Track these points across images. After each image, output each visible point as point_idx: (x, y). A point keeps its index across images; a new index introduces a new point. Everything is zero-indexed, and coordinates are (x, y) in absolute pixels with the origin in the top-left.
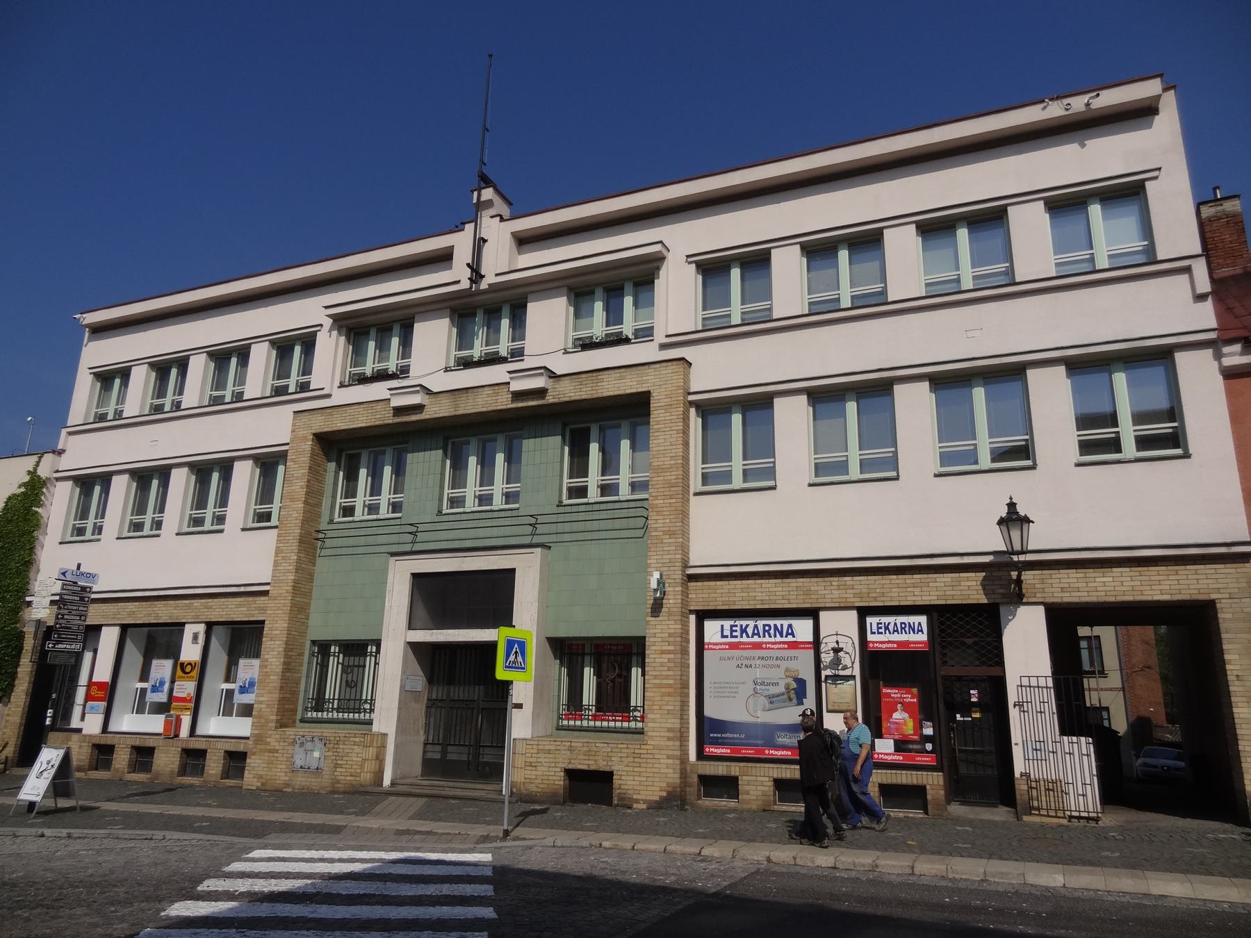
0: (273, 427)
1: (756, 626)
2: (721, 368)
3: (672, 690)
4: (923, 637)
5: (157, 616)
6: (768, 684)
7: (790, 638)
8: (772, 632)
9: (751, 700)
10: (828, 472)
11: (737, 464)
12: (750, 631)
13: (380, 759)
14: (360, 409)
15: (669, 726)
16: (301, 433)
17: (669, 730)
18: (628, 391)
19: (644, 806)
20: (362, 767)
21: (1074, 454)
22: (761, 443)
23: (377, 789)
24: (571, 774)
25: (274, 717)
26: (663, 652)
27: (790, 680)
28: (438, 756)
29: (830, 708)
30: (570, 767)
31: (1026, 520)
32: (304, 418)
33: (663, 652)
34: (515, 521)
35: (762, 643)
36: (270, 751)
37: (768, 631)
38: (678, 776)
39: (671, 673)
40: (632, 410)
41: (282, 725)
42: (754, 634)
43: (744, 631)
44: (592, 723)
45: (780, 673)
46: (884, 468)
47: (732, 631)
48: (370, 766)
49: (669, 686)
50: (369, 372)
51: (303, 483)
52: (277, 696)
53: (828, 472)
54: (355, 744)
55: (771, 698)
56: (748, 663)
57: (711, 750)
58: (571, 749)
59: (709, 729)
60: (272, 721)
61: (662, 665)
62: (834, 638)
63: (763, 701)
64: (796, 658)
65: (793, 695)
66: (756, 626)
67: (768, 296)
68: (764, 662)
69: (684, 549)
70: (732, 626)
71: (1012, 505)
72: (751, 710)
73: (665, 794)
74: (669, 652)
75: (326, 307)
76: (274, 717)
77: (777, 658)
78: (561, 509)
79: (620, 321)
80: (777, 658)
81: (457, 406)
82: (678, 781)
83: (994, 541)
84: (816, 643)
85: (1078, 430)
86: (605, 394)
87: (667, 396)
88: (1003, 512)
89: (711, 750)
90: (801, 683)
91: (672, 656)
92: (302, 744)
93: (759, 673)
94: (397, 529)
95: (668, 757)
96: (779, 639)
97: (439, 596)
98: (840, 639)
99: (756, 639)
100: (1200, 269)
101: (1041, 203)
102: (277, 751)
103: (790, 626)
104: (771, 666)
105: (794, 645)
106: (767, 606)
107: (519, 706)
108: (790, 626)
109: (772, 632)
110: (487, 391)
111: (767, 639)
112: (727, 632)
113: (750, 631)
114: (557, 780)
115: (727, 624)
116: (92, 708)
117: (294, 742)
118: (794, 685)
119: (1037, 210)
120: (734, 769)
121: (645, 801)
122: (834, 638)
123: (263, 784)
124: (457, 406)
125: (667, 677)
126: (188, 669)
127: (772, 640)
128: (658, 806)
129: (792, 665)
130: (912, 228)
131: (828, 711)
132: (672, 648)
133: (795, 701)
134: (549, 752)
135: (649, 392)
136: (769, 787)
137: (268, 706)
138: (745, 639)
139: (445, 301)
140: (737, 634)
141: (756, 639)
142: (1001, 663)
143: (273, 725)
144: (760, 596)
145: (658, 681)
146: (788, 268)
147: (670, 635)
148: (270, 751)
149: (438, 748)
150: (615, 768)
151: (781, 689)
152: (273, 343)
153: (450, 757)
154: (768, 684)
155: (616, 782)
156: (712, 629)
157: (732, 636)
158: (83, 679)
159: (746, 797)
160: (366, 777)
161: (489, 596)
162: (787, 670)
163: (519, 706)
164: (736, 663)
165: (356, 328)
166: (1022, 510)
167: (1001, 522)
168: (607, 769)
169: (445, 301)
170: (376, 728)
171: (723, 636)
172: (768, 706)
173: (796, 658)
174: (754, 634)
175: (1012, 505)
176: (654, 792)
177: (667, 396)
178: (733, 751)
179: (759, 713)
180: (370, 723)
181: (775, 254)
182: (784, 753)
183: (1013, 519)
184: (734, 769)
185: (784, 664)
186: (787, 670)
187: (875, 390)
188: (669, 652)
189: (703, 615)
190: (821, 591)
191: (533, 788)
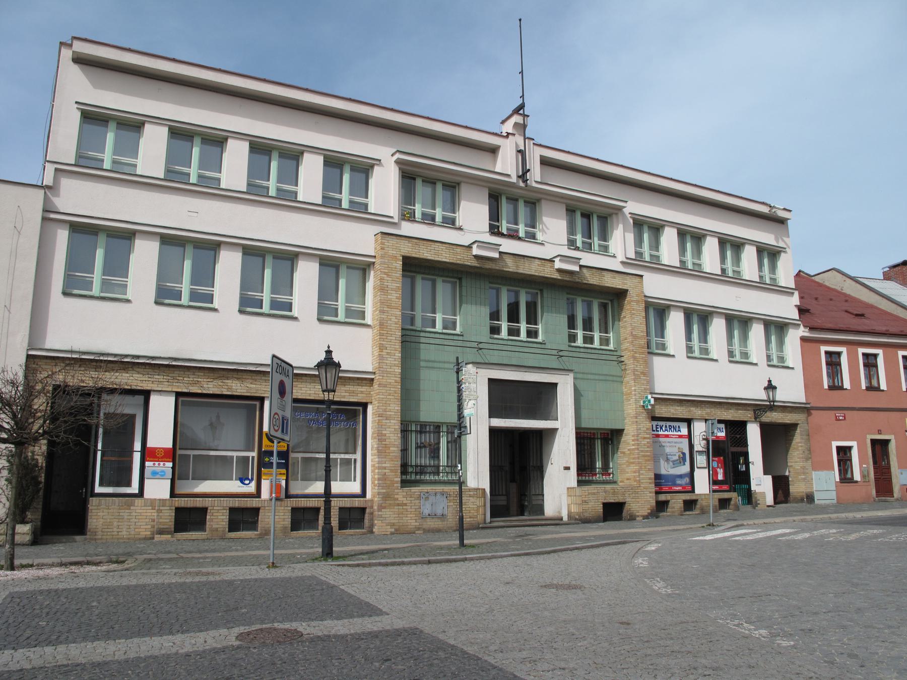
2: (657, 286)
4: (723, 434)
5: (229, 389)
7: (679, 433)
10: (165, 295)
11: (97, 276)
22: (118, 266)
26: (645, 438)
31: (775, 388)
32: (392, 241)
33: (645, 438)
36: (398, 505)
40: (613, 299)
41: (405, 483)
45: (676, 450)
46: (202, 300)
49: (648, 456)
53: (165, 295)
60: (397, 482)
67: (135, 154)
69: (650, 381)
71: (770, 381)
81: (517, 266)
83: (762, 395)
84: (689, 436)
88: (766, 384)
90: (684, 454)
92: (427, 498)
94: (460, 343)
97: (503, 397)
100: (796, 294)
102: (406, 505)
105: (681, 436)
110: (537, 262)
114: (600, 509)
116: (155, 473)
117: (419, 498)
119: (245, 146)
123: (396, 530)
125: (647, 451)
128: (645, 517)
129: (680, 446)
134: (594, 494)
135: (627, 290)
137: (392, 471)
139: (562, 198)
142: (746, 445)
143: (399, 485)
146: (236, 156)
148: (398, 505)
149: (504, 498)
150: (628, 500)
158: (137, 446)
161: (539, 398)
166: (773, 384)
167: (765, 388)
169: (562, 198)
175: (770, 381)
176: (646, 512)
181: (147, 127)
183: (770, 387)
187: (209, 248)
190: (697, 412)
191: (587, 515)
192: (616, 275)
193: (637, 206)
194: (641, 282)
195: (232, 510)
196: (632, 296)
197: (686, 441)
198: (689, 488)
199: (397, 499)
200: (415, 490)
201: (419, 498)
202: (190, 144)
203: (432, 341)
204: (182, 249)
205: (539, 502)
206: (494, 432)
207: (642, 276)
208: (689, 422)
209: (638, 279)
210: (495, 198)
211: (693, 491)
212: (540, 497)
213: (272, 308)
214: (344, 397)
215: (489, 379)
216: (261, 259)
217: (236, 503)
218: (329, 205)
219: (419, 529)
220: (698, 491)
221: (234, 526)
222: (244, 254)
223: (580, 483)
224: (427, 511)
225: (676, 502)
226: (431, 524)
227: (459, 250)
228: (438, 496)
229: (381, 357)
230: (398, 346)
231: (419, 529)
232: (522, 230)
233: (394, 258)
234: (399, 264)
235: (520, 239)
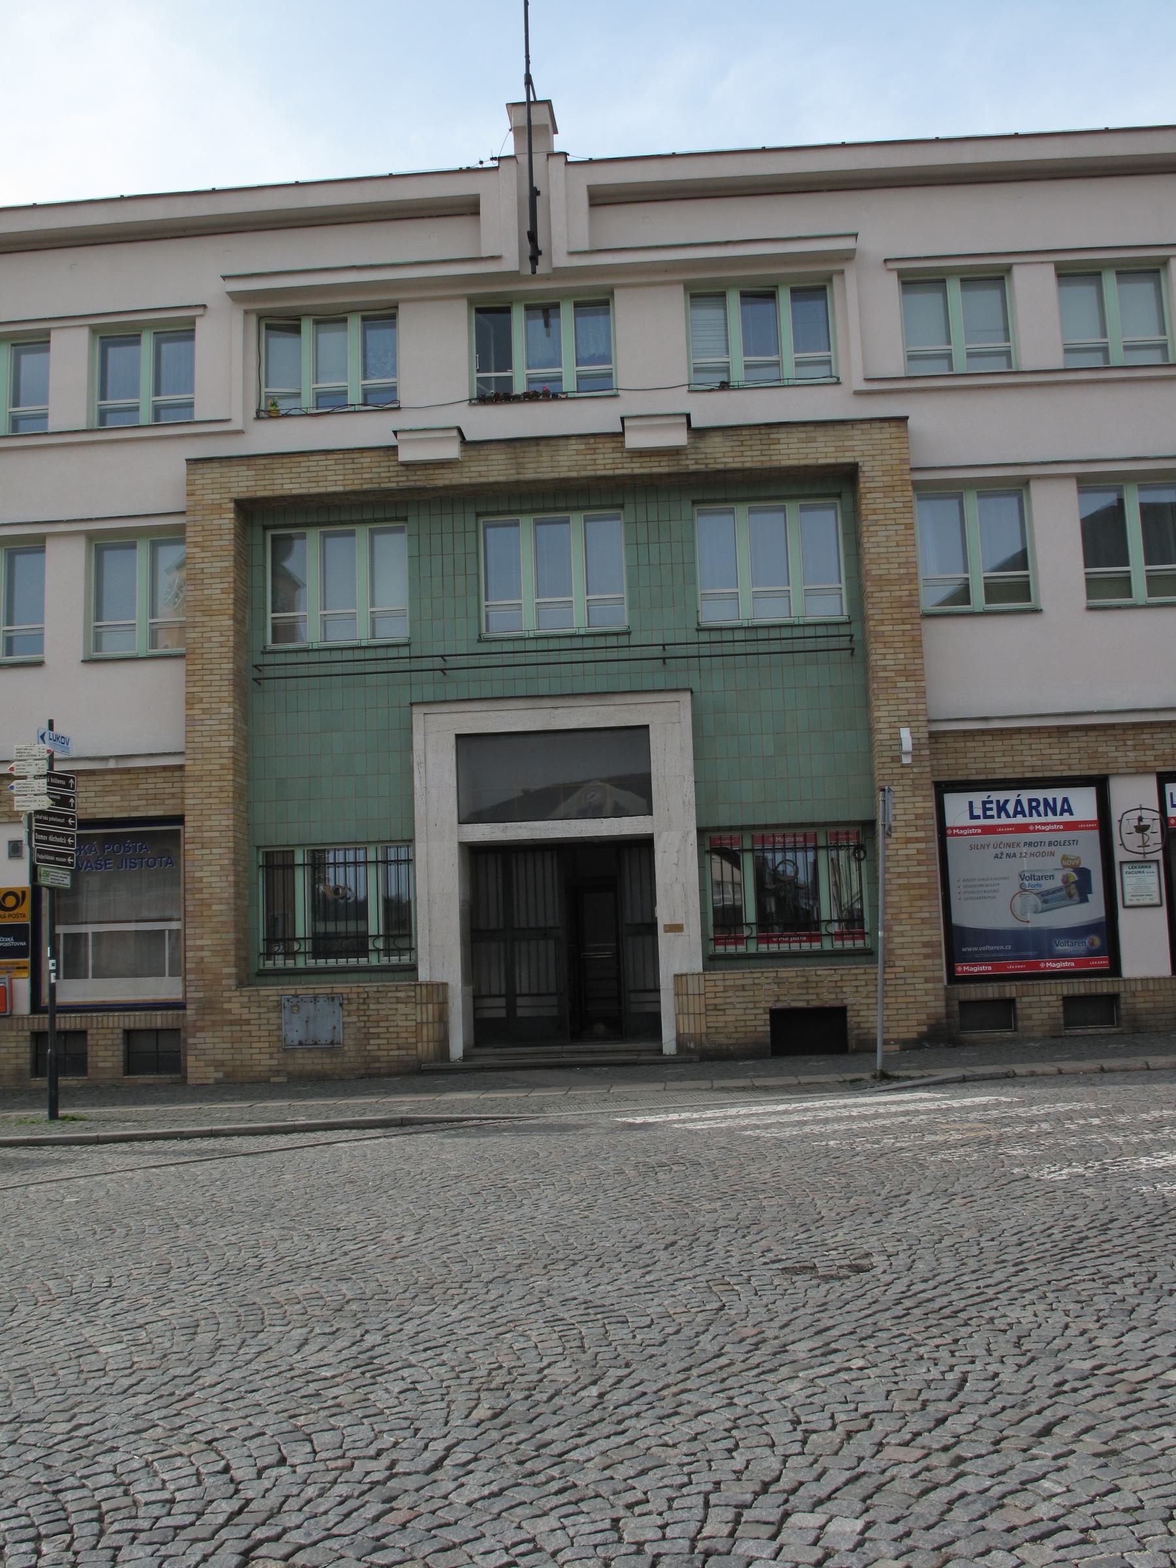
0: (144, 479)
1: (1019, 802)
3: (925, 892)
6: (1040, 878)
7: (1066, 817)
8: (1041, 808)
9: (1018, 900)
12: (1010, 808)
13: (442, 1019)
14: (330, 461)
15: (926, 939)
16: (211, 497)
17: (926, 945)
18: (822, 461)
19: (897, 1047)
20: (417, 1034)
21: (1082, 599)
23: (444, 1065)
24: (777, 1016)
25: (233, 970)
26: (908, 841)
27: (1069, 871)
28: (502, 1013)
29: (1128, 903)
30: (779, 1005)
32: (214, 473)
33: (908, 841)
34: (624, 654)
35: (1028, 825)
37: (1036, 808)
38: (943, 1003)
39: (923, 868)
42: (1016, 813)
43: (1002, 808)
44: (838, 945)
45: (1056, 862)
47: (985, 809)
48: (427, 1033)
49: (921, 886)
50: (519, 388)
51: (228, 581)
52: (232, 936)
54: (398, 1001)
55: (1045, 896)
56: (1011, 851)
57: (963, 969)
58: (779, 983)
59: (957, 941)
60: (229, 976)
61: (908, 857)
62: (1137, 813)
63: (1033, 900)
64: (1076, 842)
65: (1074, 891)
66: (1019, 802)
68: (1033, 850)
70: (984, 803)
72: (1018, 912)
73: (924, 1029)
74: (918, 840)
75: (224, 278)
76: (233, 970)
77: (1050, 844)
78: (483, 648)
79: (505, 362)
80: (1050, 844)
82: (942, 1010)
85: (1147, 563)
86: (786, 463)
87: (885, 473)
89: (888, 970)
91: (922, 845)
93: (1026, 864)
95: (927, 981)
96: (1051, 818)
98: (1145, 814)
99: (1020, 819)
101: (1051, 268)
102: (248, 1022)
103: (1065, 800)
104: (1043, 854)
106: (1040, 775)
107: (676, 928)
108: (1065, 800)
109: (1041, 808)
110: (574, 445)
111: (1035, 819)
112: (978, 811)
113: (1010, 808)
114: (762, 1025)
115: (978, 798)
117: (279, 1007)
118: (1074, 877)
120: (1010, 990)
121: (896, 1041)
122: (1137, 813)
123: (227, 1075)
124: (519, 466)
125: (918, 874)
126: (10, 902)
127: (1043, 819)
128: (912, 1046)
129: (1070, 851)
130: (1050, 271)
131: (1125, 907)
132: (922, 834)
133: (1076, 898)
134: (743, 988)
136: (1056, 1008)
137: (215, 953)
138: (1004, 820)
140: (994, 813)
141: (1020, 819)
143: (232, 982)
144: (1029, 762)
145: (905, 881)
147: (918, 817)
149: (502, 1002)
150: (850, 999)
151: (1057, 883)
152: (94, 329)
153: (521, 1013)
154: (1040, 878)
155: (852, 1019)
156: (957, 808)
157: (986, 817)
159: (1026, 1023)
160: (426, 1048)
162: (1064, 858)
163: (676, 928)
164: (992, 851)
165: (277, 318)
168: (837, 1004)
170: (423, 975)
171: (973, 817)
172: (1040, 906)
173: (1076, 842)
174: (1016, 813)
176: (912, 1026)
177: (885, 473)
178: (1078, 964)
179: (1029, 916)
180: (413, 968)
182: (1066, 964)
184: (1010, 990)
185: (1060, 851)
186: (1064, 858)
188: (918, 840)
189: (942, 788)
190: (1111, 752)
191: (722, 1040)
192: (819, 434)
193: (895, 229)
194: (904, 438)
195: (129, 1034)
196: (872, 476)
197: (1093, 838)
198: (1102, 963)
199: (229, 1011)
200: (271, 992)
201: (279, 1007)
202: (821, 303)
203: (302, 670)
204: (781, 515)
205: (649, 1008)
206: (474, 853)
207: (903, 420)
208: (1100, 784)
209: (891, 430)
210: (491, 315)
211: (1115, 969)
212: (650, 997)
213: (988, 600)
214: (136, 809)
215: (458, 736)
216: (955, 502)
217: (138, 1020)
218: (109, 422)
219: (278, 1073)
220: (1131, 968)
221: (132, 1065)
222: (1081, 490)
223: (711, 961)
224: (295, 1032)
225: (1040, 1005)
226: (306, 1062)
227: (366, 460)
228: (321, 1002)
229: (190, 721)
230: (227, 692)
231: (278, 1073)
232: (569, 374)
233: (218, 508)
234: (227, 519)
235: (517, 399)
